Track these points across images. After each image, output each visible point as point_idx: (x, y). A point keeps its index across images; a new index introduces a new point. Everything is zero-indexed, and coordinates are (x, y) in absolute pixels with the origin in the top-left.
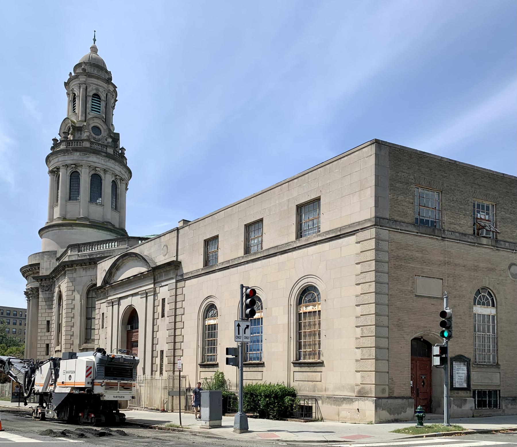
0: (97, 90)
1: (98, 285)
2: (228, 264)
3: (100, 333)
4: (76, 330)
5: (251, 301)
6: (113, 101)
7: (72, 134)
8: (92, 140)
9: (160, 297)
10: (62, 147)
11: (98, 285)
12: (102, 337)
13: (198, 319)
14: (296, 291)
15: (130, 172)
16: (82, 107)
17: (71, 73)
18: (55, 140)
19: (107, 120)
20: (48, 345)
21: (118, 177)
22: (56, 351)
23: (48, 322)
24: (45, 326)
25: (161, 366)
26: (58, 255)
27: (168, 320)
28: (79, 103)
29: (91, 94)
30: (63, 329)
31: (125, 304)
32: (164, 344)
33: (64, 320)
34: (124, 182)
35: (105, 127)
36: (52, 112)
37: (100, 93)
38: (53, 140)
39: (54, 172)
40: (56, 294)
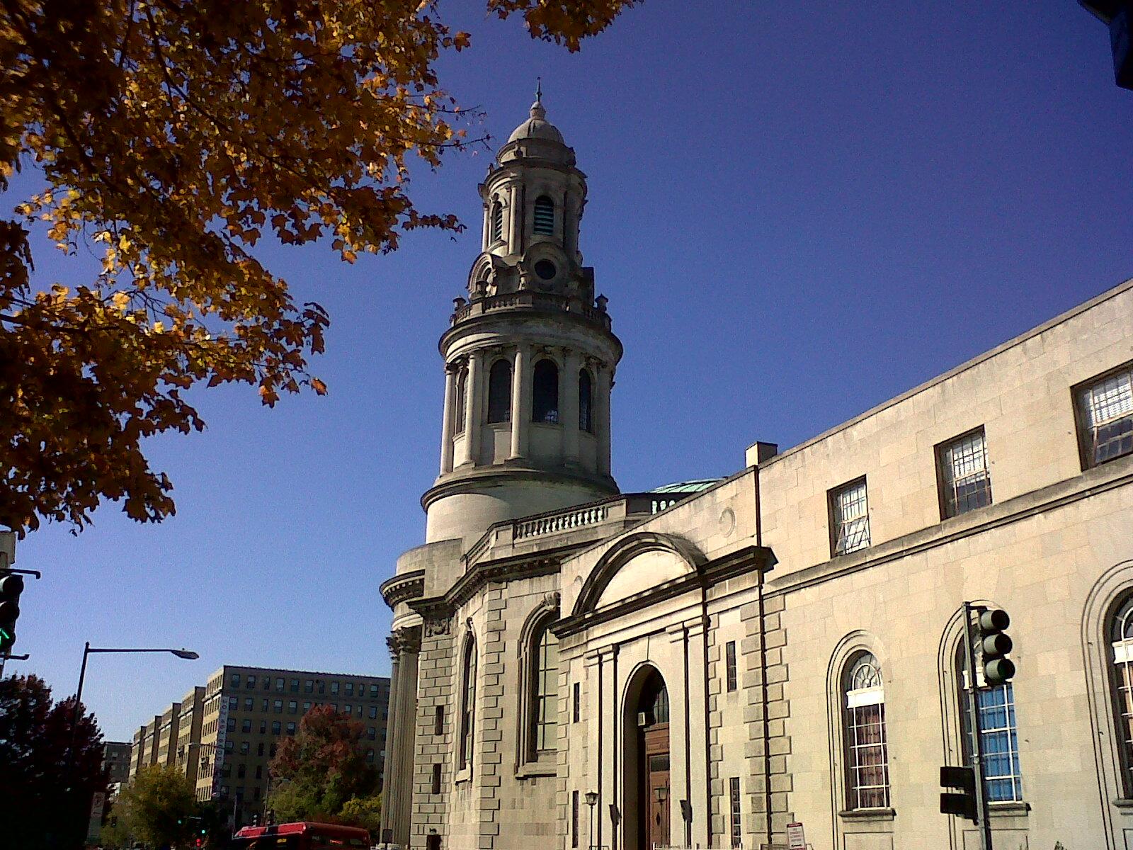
0: (546, 187)
1: (563, 616)
2: (898, 546)
3: (570, 735)
4: (509, 725)
5: (987, 639)
6: (578, 206)
8: (538, 290)
9: (720, 637)
10: (476, 311)
11: (563, 616)
12: (576, 742)
13: (828, 693)
14: (1100, 607)
19: (568, 245)
20: (437, 767)
21: (592, 360)
22: (457, 783)
23: (440, 709)
24: (431, 720)
25: (736, 820)
26: (466, 548)
27: (746, 696)
29: (535, 197)
30: (478, 727)
31: (630, 660)
32: (738, 762)
33: (479, 705)
34: (606, 370)
35: (563, 258)
37: (552, 194)
39: (457, 366)
40: (459, 642)
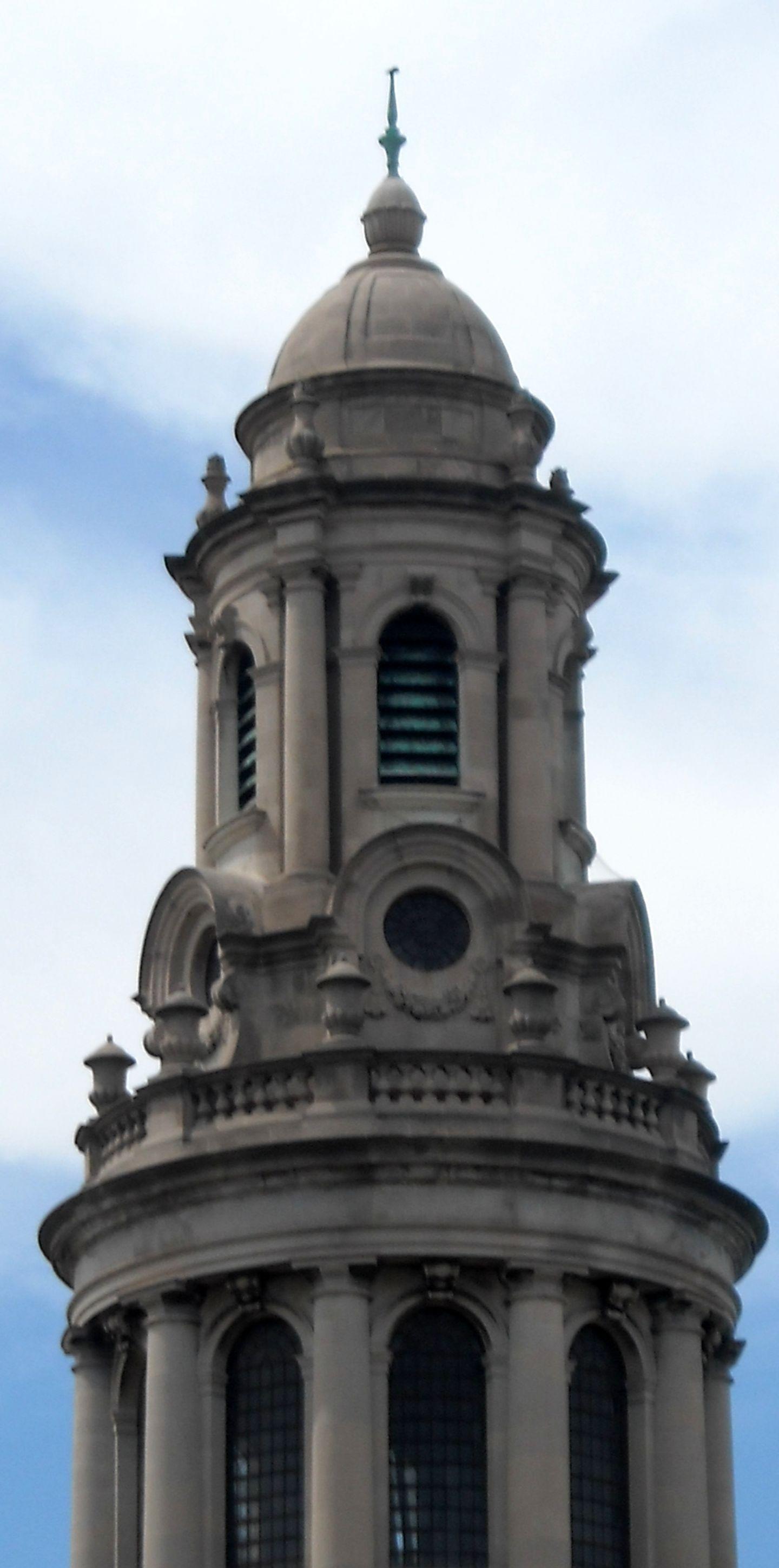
7: (228, 1005)
15: (592, 546)
16: (306, 778)
17: (216, 463)
18: (109, 1064)
21: (623, 1292)
28: (284, 713)
36: (202, 470)
38: (88, 1063)
